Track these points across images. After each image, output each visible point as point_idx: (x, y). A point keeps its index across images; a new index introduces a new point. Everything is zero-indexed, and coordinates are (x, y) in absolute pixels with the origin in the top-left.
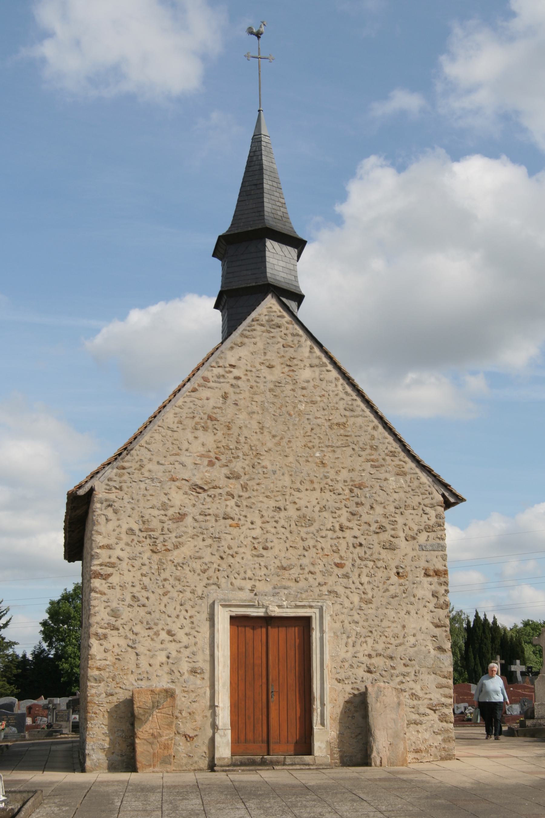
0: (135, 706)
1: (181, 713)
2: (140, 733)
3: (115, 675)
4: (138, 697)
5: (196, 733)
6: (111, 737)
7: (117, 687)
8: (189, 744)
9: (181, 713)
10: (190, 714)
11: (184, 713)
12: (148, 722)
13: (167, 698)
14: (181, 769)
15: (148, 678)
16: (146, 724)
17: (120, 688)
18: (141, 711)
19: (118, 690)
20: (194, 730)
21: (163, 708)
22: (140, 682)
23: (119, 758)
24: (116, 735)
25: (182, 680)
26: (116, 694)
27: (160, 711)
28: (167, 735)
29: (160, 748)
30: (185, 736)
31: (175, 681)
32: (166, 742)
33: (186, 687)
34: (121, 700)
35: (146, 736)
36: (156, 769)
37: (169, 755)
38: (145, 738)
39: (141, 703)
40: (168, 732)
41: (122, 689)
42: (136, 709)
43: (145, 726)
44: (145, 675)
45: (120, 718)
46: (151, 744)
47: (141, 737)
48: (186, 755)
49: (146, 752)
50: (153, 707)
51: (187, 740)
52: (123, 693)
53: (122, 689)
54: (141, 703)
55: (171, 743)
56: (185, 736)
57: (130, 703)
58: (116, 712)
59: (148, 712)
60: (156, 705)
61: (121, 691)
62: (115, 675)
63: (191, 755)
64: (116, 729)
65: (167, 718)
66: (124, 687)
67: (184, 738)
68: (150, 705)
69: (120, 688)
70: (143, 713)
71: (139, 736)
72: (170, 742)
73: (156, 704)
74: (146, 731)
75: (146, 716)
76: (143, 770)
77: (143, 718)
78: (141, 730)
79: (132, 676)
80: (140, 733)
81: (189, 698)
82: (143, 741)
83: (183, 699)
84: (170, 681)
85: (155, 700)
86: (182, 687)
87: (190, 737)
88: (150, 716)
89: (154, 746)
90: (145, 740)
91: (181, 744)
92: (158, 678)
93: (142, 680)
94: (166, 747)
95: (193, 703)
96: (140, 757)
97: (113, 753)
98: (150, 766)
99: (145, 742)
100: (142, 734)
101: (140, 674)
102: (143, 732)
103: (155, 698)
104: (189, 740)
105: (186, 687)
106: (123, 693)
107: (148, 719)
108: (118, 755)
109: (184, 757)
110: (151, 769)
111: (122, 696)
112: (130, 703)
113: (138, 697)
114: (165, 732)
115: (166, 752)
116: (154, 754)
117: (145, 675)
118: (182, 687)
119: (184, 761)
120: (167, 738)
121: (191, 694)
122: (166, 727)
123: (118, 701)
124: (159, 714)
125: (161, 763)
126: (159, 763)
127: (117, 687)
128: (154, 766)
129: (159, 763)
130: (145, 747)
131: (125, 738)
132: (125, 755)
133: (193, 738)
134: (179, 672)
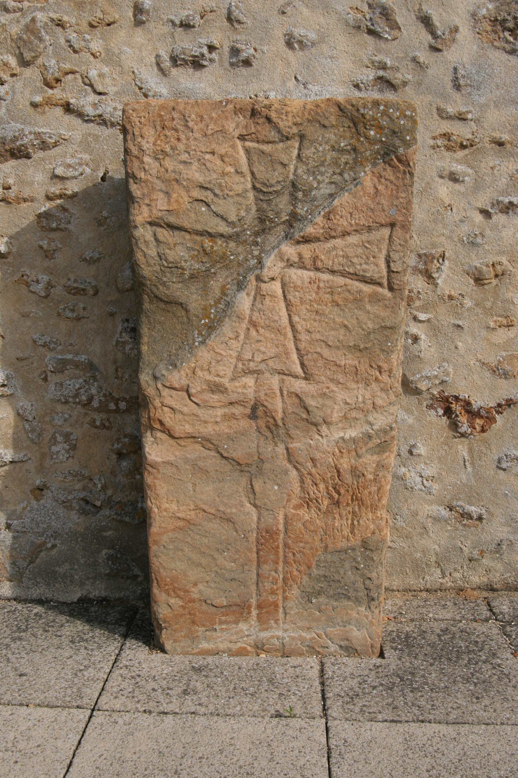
0: (141, 215)
1: (429, 276)
2: (171, 398)
3: (31, 28)
4: (160, 155)
5: (506, 390)
6: (25, 403)
7: (50, 103)
8: (462, 448)
9: (429, 276)
10: (479, 280)
11: (449, 280)
12: (227, 329)
13: (357, 163)
14: (412, 581)
15: (235, 51)
16: (213, 341)
17: (68, 108)
18: (180, 250)
19: (55, 124)
20: (498, 371)
21: (329, 237)
22: (186, 79)
23: (75, 520)
24: (52, 391)
25: (438, 70)
26: (44, 146)
27: (306, 250)
28: (350, 413)
29: (308, 502)
30: (448, 406)
31: (397, 78)
32: (345, 464)
33: (461, 118)
34: (73, 187)
35: (213, 419)
36: (279, 632)
37: (365, 544)
38: (209, 430)
39: (182, 198)
40: (360, 393)
41: (80, 115)
42: (143, 233)
43: (204, 355)
44: (218, 35)
45: (77, 292)
46: (249, 469)
47: (183, 428)
48: (445, 513)
49: (214, 526)
50: (264, 224)
51: (454, 426)
52: (85, 145)
53: (80, 115)
54: (182, 198)
55: (381, 466)
56: (448, 406)
57: (111, 204)
58: (48, 254)
59: (231, 255)
60: (280, 214)
61: (73, 129)
62: (31, 28)
63: (473, 509)
64: (50, 360)
65: (358, 300)
66: (87, 102)
67: (436, 418)
68: (239, 206)
69: (68, 108)
70: (192, 265)
71: (167, 417)
72: (369, 461)
73: (283, 203)
74: (216, 388)
75: (215, 285)
76: (193, 638)
77: (193, 299)
78: (177, 378)
79: (139, 36)
80: (171, 398)
81: (478, 186)
82: (195, 451)
83: (444, 190)
84: (371, 75)
85: (275, 176)
86: (442, 114)
87: (473, 414)
88: (240, 286)
89: (268, 489)
90: (206, 442)
91: (422, 449)
92: (294, 58)
93: (197, 63)
94: (347, 492)
95: (499, 218)
96: (175, 560)
97: (39, 491)
98: (239, 610)
99: (211, 460)
100: (189, 408)
101: (186, 26)
102: (200, 389)
103: (274, 162)
104: (465, 428)
105: (461, 118)
106: (85, 145)
107: (226, 307)
108: (66, 504)
109: (436, 519)
110: (248, 630)
111: (80, 157)
112: (111, 204)
113: (160, 155)
114: (341, 395)
115: (341, 523)
116: (266, 536)
117: (218, 35)
118: (442, 114)
119: (435, 541)
120: (352, 433)
121: (491, 160)
122: (348, 360)
123: (55, 189)
124: (298, 275)
125: (308, 596)
126: (295, 592)
127: (50, 103)
128: (267, 611)
129: (295, 592)
130: (207, 492)
131: (103, 408)
132: (108, 502)
133: (491, 420)
134: (426, 21)
